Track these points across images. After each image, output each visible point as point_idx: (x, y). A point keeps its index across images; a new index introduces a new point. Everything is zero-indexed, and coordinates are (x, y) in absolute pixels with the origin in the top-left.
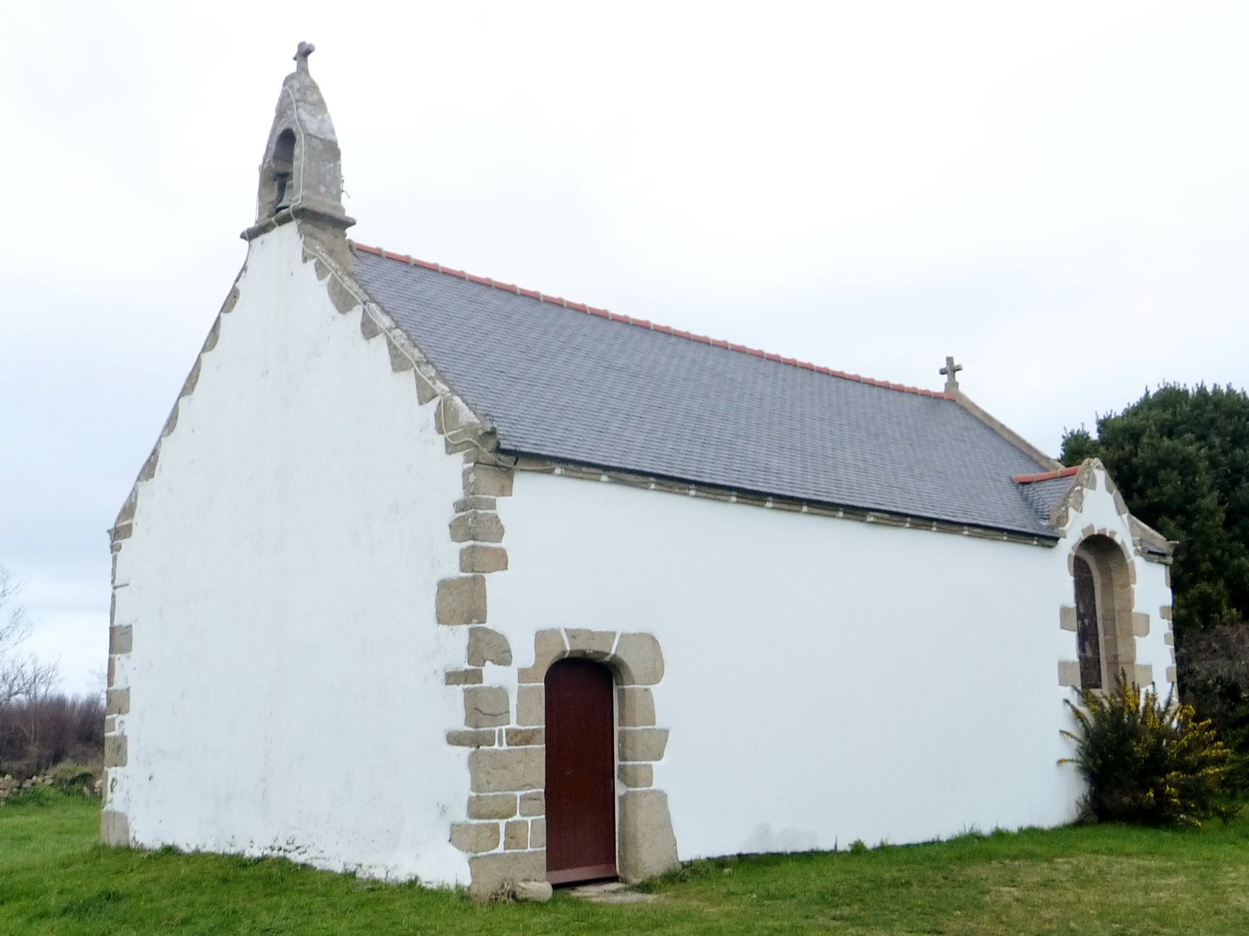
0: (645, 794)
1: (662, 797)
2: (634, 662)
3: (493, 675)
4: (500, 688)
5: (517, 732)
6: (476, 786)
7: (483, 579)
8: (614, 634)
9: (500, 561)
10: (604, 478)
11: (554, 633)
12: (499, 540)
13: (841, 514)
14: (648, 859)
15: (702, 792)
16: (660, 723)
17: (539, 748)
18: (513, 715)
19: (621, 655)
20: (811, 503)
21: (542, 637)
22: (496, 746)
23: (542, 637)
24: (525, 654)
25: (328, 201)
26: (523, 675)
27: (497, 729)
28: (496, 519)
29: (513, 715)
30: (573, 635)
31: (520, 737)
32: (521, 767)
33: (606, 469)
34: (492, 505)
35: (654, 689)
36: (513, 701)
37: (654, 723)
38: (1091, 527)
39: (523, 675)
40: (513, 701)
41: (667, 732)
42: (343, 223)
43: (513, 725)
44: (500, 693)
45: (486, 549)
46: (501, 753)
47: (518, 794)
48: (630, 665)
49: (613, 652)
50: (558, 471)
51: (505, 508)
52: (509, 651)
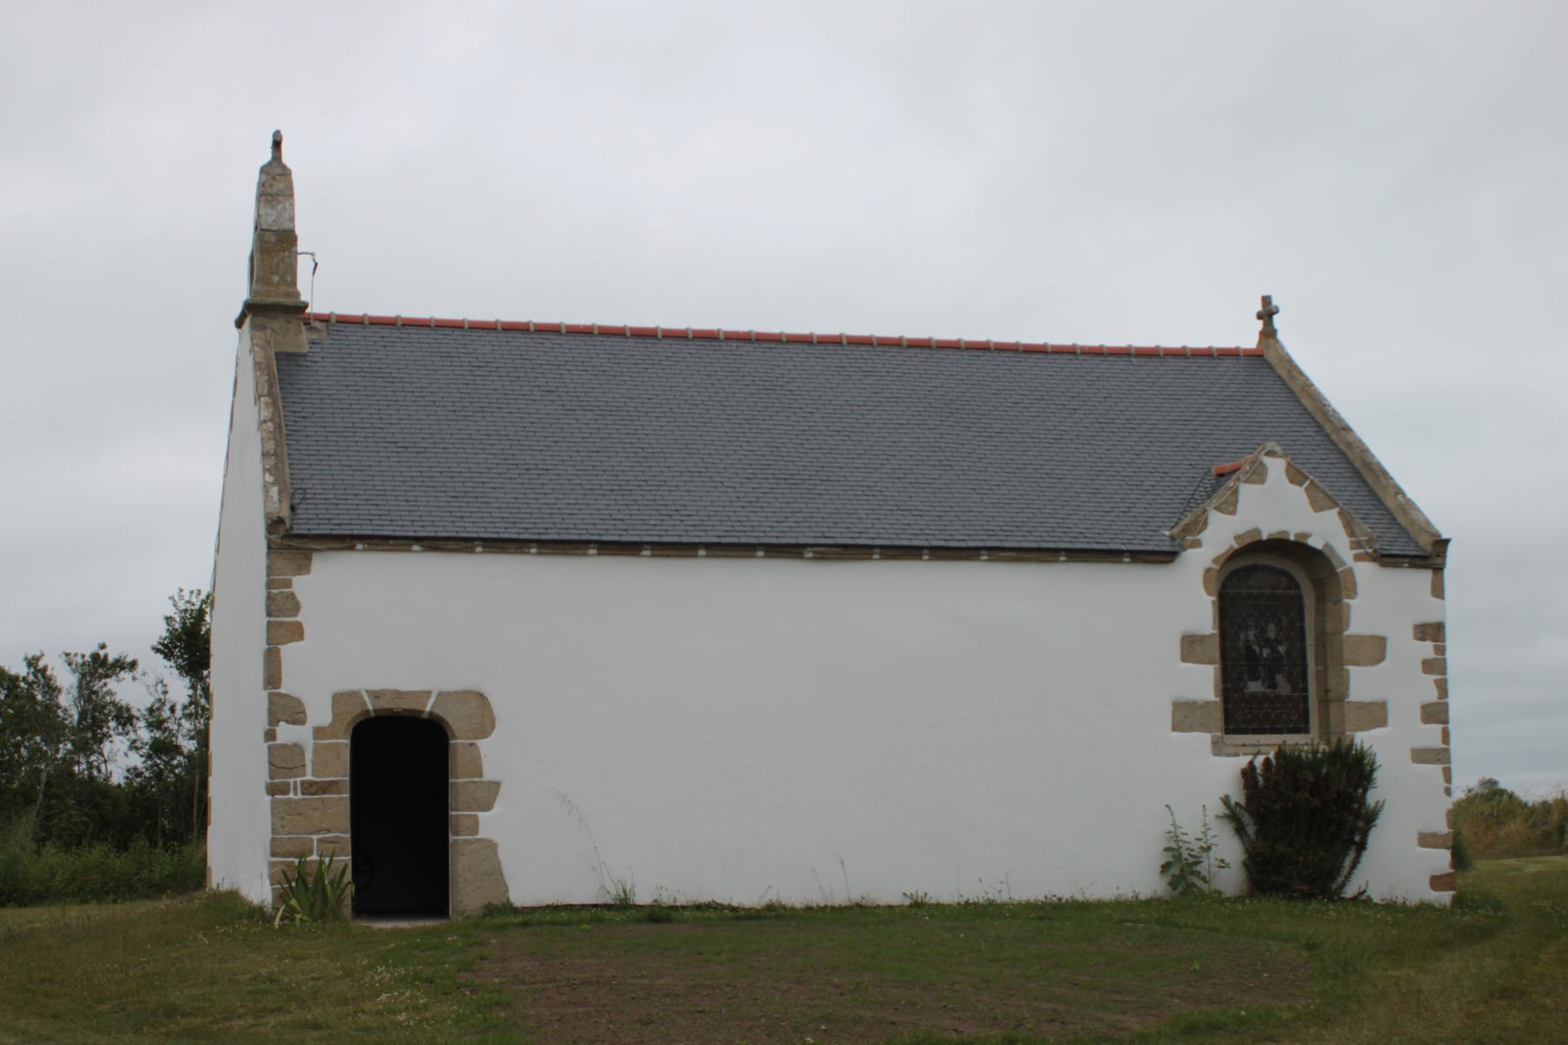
0: (469, 842)
1: (491, 846)
2: (454, 719)
3: (287, 733)
4: (295, 745)
5: (312, 783)
6: (274, 831)
7: (278, 651)
8: (429, 693)
9: (297, 632)
10: (416, 547)
11: (353, 695)
12: (296, 614)
13: (533, 550)
14: (466, 895)
15: (535, 837)
16: (489, 774)
17: (342, 799)
18: (309, 768)
19: (438, 711)
20: (708, 546)
21: (339, 699)
22: (291, 795)
23: (339, 699)
24: (320, 713)
25: (283, 289)
26: (319, 732)
27: (292, 781)
28: (292, 596)
29: (309, 768)
30: (376, 695)
31: (314, 789)
32: (318, 813)
33: (417, 540)
34: (289, 584)
35: (483, 744)
36: (309, 756)
37: (480, 775)
38: (1308, 536)
39: (319, 732)
40: (309, 756)
41: (498, 784)
42: (306, 306)
43: (309, 777)
44: (296, 749)
45: (281, 623)
46: (296, 802)
47: (315, 837)
48: (451, 721)
49: (428, 709)
50: (360, 546)
51: (301, 585)
52: (304, 712)
